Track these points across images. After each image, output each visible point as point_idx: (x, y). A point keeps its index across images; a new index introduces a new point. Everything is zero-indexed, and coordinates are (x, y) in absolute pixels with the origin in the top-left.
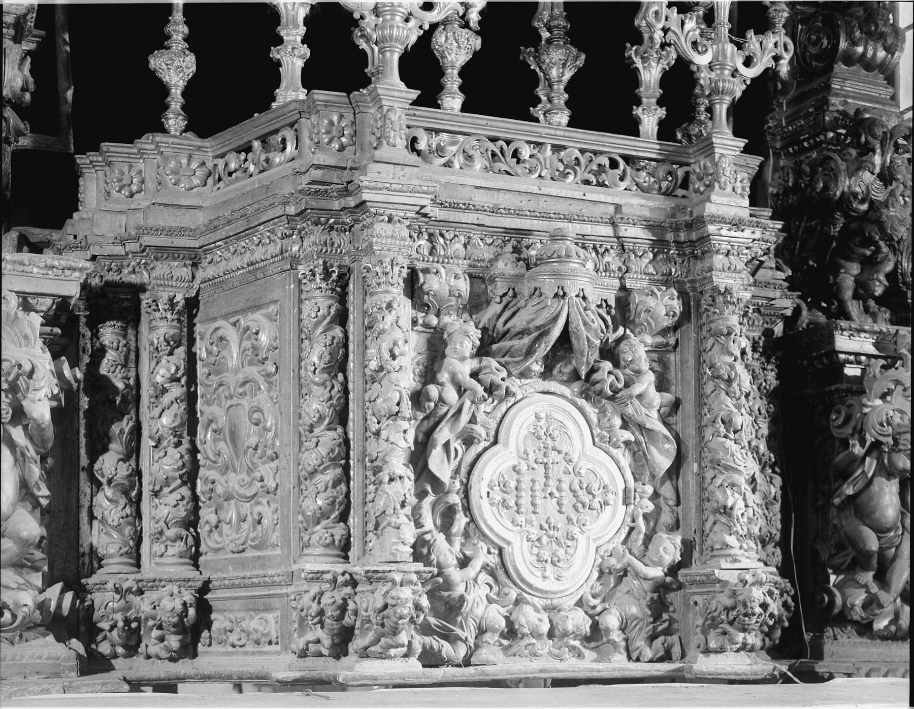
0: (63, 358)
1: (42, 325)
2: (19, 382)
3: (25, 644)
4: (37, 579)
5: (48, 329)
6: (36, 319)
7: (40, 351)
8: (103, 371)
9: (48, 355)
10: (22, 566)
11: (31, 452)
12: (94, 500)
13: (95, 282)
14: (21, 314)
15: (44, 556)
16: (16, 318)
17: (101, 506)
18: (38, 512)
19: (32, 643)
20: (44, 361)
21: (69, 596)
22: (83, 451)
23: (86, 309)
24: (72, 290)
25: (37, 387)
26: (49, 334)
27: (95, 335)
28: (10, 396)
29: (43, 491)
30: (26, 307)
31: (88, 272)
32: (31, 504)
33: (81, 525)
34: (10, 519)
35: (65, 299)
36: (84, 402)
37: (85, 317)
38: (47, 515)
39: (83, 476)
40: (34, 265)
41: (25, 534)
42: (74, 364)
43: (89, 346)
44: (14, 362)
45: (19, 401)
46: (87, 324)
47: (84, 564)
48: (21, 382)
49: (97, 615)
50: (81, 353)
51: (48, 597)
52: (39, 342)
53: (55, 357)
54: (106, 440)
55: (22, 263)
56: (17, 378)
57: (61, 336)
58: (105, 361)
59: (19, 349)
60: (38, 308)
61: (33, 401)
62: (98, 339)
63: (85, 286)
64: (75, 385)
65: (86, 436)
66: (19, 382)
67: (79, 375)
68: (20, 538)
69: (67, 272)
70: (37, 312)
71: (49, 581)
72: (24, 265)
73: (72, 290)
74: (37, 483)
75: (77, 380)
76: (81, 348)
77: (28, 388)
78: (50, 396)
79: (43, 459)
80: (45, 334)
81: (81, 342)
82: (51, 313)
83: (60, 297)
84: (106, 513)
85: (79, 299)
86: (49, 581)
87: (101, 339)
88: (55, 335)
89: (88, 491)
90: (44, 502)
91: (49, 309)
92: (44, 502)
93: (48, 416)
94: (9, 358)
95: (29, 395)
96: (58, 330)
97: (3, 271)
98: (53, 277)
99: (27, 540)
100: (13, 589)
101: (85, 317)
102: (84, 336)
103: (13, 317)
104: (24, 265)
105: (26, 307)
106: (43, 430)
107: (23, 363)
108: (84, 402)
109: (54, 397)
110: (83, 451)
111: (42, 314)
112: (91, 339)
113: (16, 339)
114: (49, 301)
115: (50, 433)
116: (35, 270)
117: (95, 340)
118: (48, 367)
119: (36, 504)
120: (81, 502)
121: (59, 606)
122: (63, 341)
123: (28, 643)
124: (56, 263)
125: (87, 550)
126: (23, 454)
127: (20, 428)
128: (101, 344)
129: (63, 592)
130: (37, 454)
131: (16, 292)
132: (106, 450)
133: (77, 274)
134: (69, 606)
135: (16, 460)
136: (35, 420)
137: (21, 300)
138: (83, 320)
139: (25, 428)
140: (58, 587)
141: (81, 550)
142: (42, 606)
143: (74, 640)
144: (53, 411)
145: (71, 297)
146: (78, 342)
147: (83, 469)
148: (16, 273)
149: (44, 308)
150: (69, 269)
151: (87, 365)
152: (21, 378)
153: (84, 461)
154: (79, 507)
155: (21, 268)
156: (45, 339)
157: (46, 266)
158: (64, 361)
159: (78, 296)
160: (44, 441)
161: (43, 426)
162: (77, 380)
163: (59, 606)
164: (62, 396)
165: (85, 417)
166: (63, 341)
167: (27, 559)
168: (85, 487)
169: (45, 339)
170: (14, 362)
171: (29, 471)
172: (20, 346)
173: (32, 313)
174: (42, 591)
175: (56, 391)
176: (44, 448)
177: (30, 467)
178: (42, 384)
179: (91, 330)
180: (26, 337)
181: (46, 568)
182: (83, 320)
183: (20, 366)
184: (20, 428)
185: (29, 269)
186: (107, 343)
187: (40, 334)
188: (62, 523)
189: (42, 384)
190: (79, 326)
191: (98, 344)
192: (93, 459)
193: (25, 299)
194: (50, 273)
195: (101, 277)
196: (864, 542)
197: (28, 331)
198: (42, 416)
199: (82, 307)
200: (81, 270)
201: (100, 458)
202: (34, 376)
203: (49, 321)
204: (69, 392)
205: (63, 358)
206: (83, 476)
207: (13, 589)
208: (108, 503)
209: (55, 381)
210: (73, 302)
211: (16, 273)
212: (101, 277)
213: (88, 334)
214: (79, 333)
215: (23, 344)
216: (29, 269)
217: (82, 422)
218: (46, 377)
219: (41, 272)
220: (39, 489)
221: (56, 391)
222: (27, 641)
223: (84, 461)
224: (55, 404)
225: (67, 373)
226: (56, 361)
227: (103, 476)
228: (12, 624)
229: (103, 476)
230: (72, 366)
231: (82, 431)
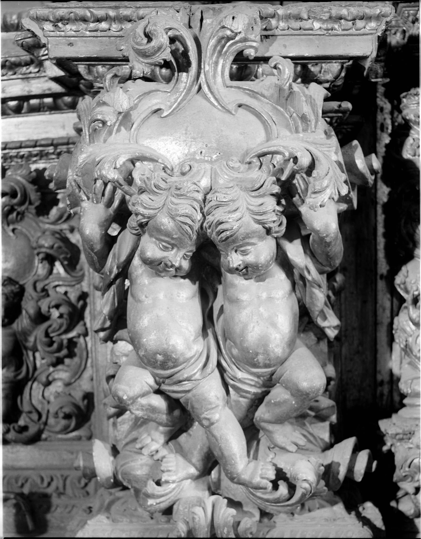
0: (355, 142)
1: (326, 99)
2: (295, 181)
3: (307, 515)
4: (323, 432)
5: (334, 105)
6: (317, 92)
7: (323, 136)
8: (407, 154)
9: (334, 140)
10: (303, 416)
11: (313, 274)
12: (396, 320)
13: (395, 39)
14: (297, 87)
15: (331, 403)
16: (291, 93)
17: (405, 331)
18: (324, 346)
19: (317, 513)
20: (328, 151)
21: (363, 457)
22: (381, 254)
23: (384, 76)
24: (364, 47)
25: (318, 188)
26: (336, 112)
27: (397, 108)
28: (283, 202)
29: (331, 324)
30: (306, 77)
31: (388, 19)
32: (315, 335)
33: (378, 347)
34: (286, 364)
35: (357, 61)
36: (383, 192)
37: (384, 85)
38: (334, 351)
39: (381, 285)
40: (315, 18)
41: (304, 385)
42: (368, 150)
43: (389, 122)
44: (287, 154)
45: (294, 205)
46: (386, 95)
47: (382, 395)
48: (298, 182)
49: (398, 474)
50: (379, 132)
51: (336, 460)
52: (323, 125)
53: (344, 142)
54: (411, 246)
55: (298, 18)
56: (292, 176)
57: (352, 112)
58: (410, 141)
59: (295, 135)
60: (322, 77)
61: (312, 208)
62: (400, 112)
63: (382, 42)
64: (371, 179)
65: (385, 235)
66: (295, 181)
67: (377, 164)
68: (298, 390)
69: (360, 24)
70: (319, 82)
71: (338, 435)
72: (301, 19)
73: (364, 47)
74: (322, 312)
75: (373, 172)
76: (379, 125)
77: (307, 189)
78: (336, 197)
79: (331, 277)
80: (331, 112)
81: (380, 118)
82: (339, 82)
83: (350, 58)
84: (410, 339)
85: (377, 60)
86: (338, 435)
87: (405, 112)
88: (344, 112)
89: (388, 304)
90: (332, 333)
91: (336, 78)
92: (332, 333)
93: (333, 225)
94: (281, 149)
95: (308, 200)
96: (347, 105)
97: (228, 7)
98: (340, 32)
99: (307, 394)
100: (292, 452)
101: (384, 85)
102: (382, 109)
103: (287, 92)
104: (301, 19)
105: (306, 77)
106: (328, 244)
107: (298, 155)
108: (383, 192)
109: (343, 199)
110: (381, 254)
111: (327, 85)
112: (392, 113)
113: (291, 122)
114: (335, 67)
115: (338, 248)
116: (317, 25)
117: (396, 114)
118: (334, 158)
119: (321, 334)
120: (379, 318)
121: (350, 469)
122: (355, 119)
123: (312, 514)
124: (344, 12)
125: (386, 378)
126: (302, 278)
127: (298, 243)
128: (404, 119)
129: (356, 450)
130: (321, 273)
131: (292, 59)
132: (410, 257)
133: (373, 24)
134: (363, 471)
135: (294, 284)
136: (317, 232)
137: (299, 68)
138: (381, 89)
139: (305, 240)
140: (349, 443)
141: (379, 378)
142: (328, 473)
143: (369, 505)
144: (343, 217)
145: (365, 58)
146: (375, 117)
147: (382, 277)
148: (291, 32)
149: (330, 77)
150: (362, 18)
151: (387, 146)
152: (298, 176)
153: (383, 267)
154: (376, 324)
155: (297, 24)
156: (331, 118)
157: (330, 18)
158: (356, 147)
159: (374, 54)
160: (329, 258)
161: (328, 240)
162: (373, 172)
163: (350, 469)
164: (354, 196)
165: (384, 212)
166: (355, 119)
167: (311, 409)
168: (385, 300)
169: (331, 118)
170: (287, 154)
171: (311, 298)
172: (297, 131)
173: (313, 85)
174: (329, 446)
175: (344, 191)
176: (330, 266)
177: (312, 293)
178: (325, 183)
179: (391, 102)
180: (304, 118)
181: (334, 418)
182: (381, 89)
183: (295, 159)
184: (298, 243)
185: (307, 24)
186: (411, 117)
187: (324, 112)
188: (356, 342)
189: (325, 183)
190: (377, 97)
191: (400, 119)
192: (394, 270)
193: (304, 67)
194: (336, 26)
195: (404, 32)
196: (214, 44)
197: (306, 109)
198: (327, 226)
199: (380, 71)
200: (378, 18)
201: (404, 269)
202: (315, 173)
203: (335, 93)
204: (363, 189)
205: (355, 142)
206: (381, 285)
207: (292, 452)
208: (413, 327)
209: (344, 177)
210: (367, 64)
211: (291, 32)
212: (404, 32)
213: (388, 106)
214: (376, 106)
215: (300, 129)
216: (307, 24)
217: (381, 218)
218: (331, 173)
219: (325, 26)
220: (325, 318)
221: (344, 191)
222: (310, 511)
223: (383, 267)
224: (344, 207)
225: (360, 162)
226: (346, 147)
227: (407, 292)
228: (289, 499)
229: (407, 292)
230: (366, 153)
231: (381, 230)
